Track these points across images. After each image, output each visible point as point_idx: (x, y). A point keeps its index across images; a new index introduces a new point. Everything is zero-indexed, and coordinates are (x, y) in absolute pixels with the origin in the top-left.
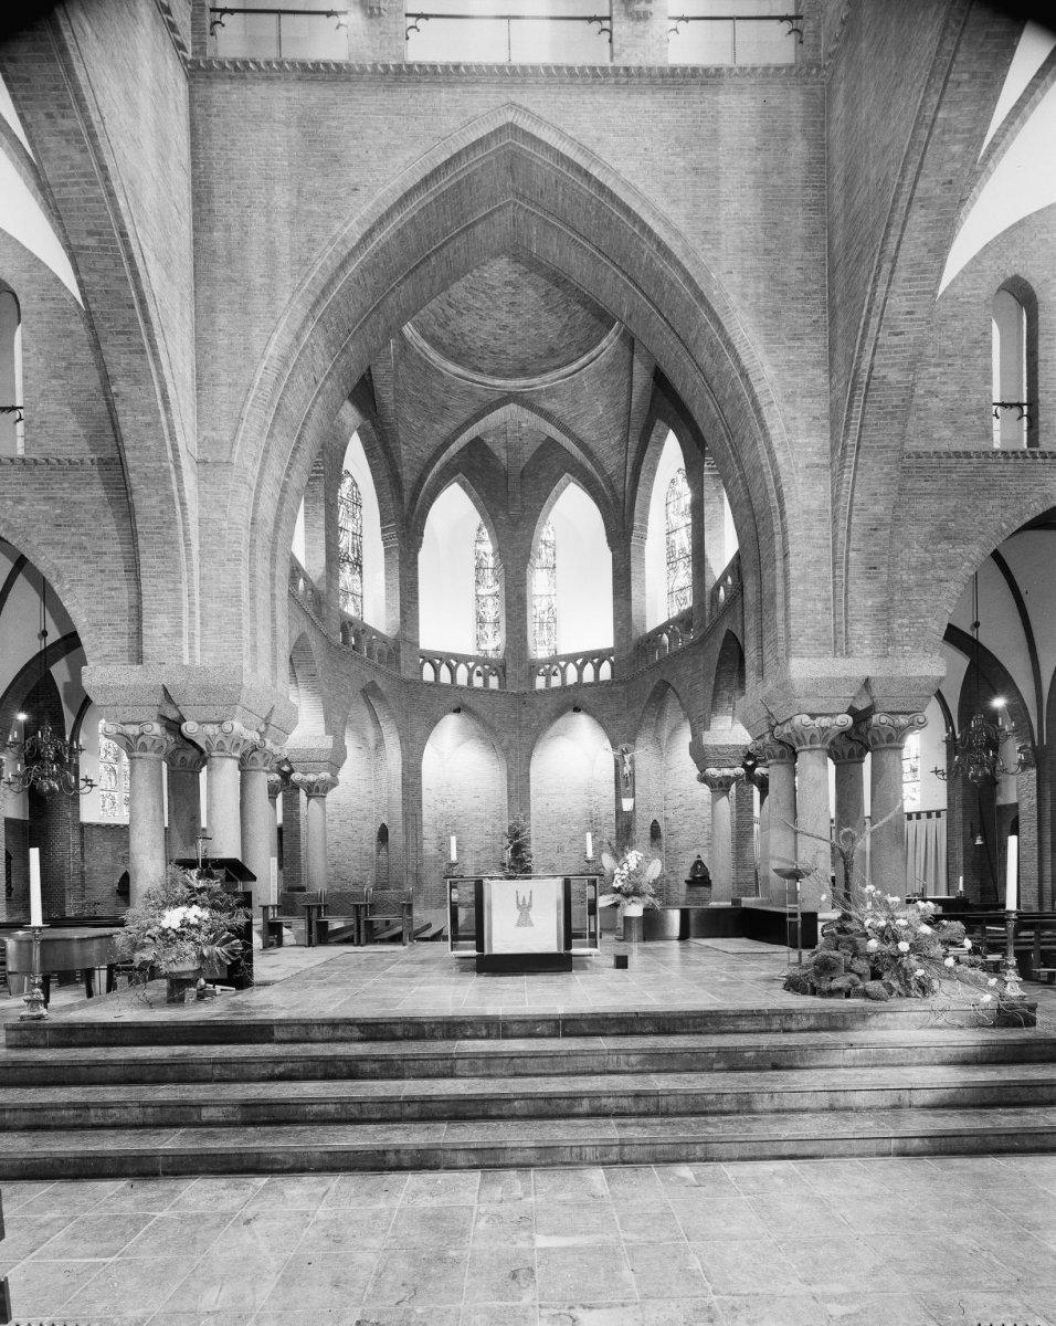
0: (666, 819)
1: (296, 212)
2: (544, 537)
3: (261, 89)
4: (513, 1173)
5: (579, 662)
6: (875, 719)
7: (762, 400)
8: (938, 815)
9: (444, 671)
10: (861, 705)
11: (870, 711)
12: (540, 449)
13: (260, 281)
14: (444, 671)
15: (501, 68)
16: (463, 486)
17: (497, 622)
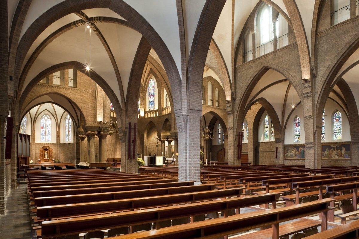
0: (148, 146)
6: (101, 132)
10: (99, 131)
11: (100, 132)
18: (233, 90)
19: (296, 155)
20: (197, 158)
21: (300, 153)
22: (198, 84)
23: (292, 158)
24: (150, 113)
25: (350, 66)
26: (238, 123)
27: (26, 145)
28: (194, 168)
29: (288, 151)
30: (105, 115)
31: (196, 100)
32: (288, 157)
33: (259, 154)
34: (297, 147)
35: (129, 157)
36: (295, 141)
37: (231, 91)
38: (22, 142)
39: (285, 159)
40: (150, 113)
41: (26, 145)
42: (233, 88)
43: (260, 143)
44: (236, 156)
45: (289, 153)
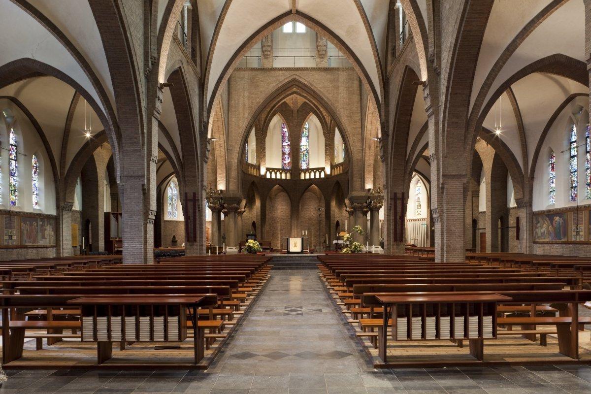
1: (249, 97)
2: (305, 126)
3: (243, 73)
4: (360, 105)
5: (315, 171)
7: (348, 136)
8: (425, 220)
9: (273, 174)
12: (303, 104)
13: (241, 111)
14: (273, 174)
15: (293, 68)
16: (279, 115)
17: (289, 154)
18: (383, 119)
19: (549, 233)
20: (138, 242)
21: (555, 229)
22: (135, 140)
23: (543, 240)
24: (310, 173)
25: (521, 32)
26: (393, 176)
27: (118, 224)
28: (132, 255)
29: (537, 224)
30: (230, 180)
31: (135, 162)
32: (538, 238)
33: (508, 231)
34: (550, 214)
35: (395, 240)
36: (551, 203)
37: (381, 121)
38: (117, 222)
39: (535, 243)
40: (310, 173)
41: (118, 224)
42: (383, 114)
43: (509, 208)
44: (392, 236)
45: (539, 228)
